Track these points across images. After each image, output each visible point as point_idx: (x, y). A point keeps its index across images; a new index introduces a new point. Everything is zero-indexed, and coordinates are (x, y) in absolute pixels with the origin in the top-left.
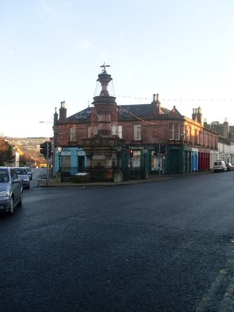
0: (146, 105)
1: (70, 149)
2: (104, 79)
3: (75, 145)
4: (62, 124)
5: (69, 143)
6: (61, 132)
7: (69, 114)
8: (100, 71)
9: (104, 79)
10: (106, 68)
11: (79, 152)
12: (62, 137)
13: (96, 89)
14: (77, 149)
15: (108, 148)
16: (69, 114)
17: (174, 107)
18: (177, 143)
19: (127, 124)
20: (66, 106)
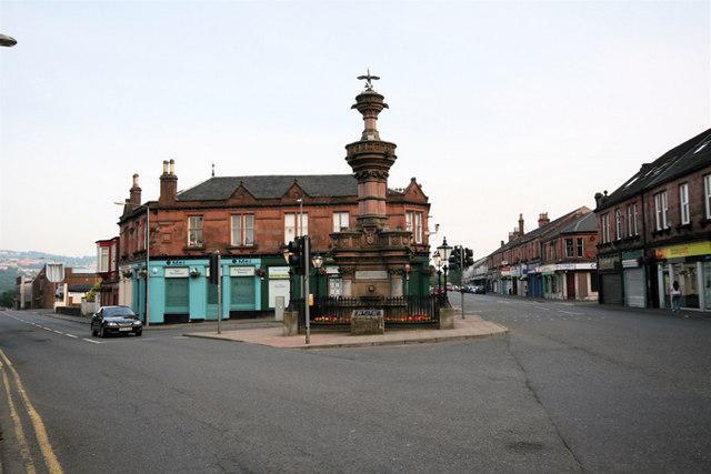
0: (262, 178)
1: (187, 262)
2: (369, 104)
3: (199, 254)
4: (168, 209)
5: (186, 250)
6: (166, 226)
7: (183, 185)
8: (360, 88)
9: (369, 104)
10: (372, 81)
11: (232, 269)
12: (167, 237)
13: (353, 128)
14: (164, 263)
15: (401, 254)
16: (183, 185)
17: (413, 180)
18: (419, 249)
19: (320, 212)
20: (177, 171)
